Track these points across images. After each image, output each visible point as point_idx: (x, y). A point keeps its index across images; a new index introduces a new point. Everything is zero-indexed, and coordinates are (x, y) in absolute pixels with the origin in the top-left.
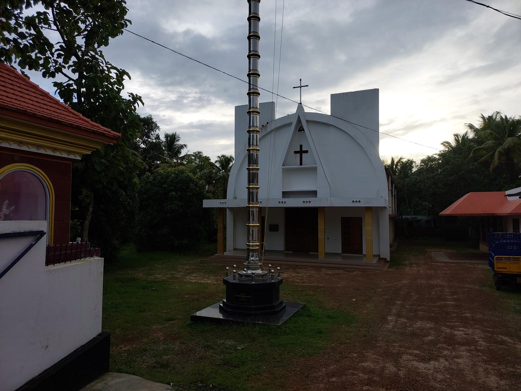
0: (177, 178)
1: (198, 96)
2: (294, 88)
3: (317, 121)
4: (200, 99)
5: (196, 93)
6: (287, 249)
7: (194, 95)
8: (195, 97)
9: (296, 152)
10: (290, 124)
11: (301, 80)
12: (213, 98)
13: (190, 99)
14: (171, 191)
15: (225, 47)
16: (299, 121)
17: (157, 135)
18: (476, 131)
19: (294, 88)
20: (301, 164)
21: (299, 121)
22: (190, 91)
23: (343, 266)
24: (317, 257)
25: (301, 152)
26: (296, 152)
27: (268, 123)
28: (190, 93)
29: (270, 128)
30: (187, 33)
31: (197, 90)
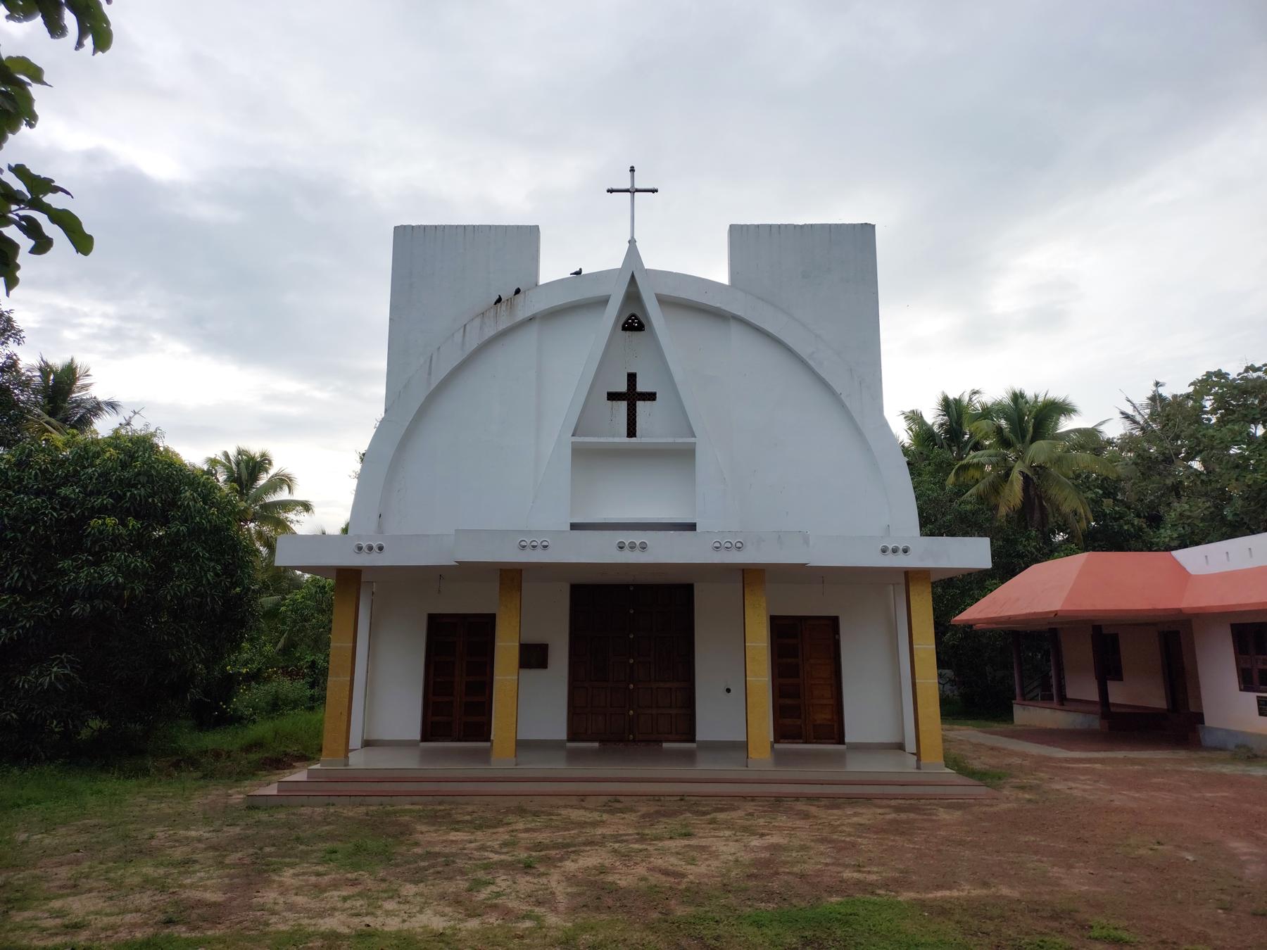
0: (124, 465)
1: (112, 323)
2: (610, 191)
3: (694, 305)
4: (116, 335)
5: (105, 315)
6: (573, 735)
7: (98, 321)
8: (100, 327)
9: (613, 396)
10: (603, 302)
11: (632, 170)
12: (157, 337)
13: (85, 330)
14: (103, 511)
15: (206, 212)
16: (633, 295)
17: (9, 357)
18: (1036, 401)
19: (610, 191)
20: (632, 432)
21: (633, 295)
22: (86, 309)
23: (939, 790)
24: (485, 756)
25: (632, 396)
26: (613, 396)
27: (518, 291)
28: (86, 315)
29: (526, 308)
30: (92, 157)
31: (110, 309)
